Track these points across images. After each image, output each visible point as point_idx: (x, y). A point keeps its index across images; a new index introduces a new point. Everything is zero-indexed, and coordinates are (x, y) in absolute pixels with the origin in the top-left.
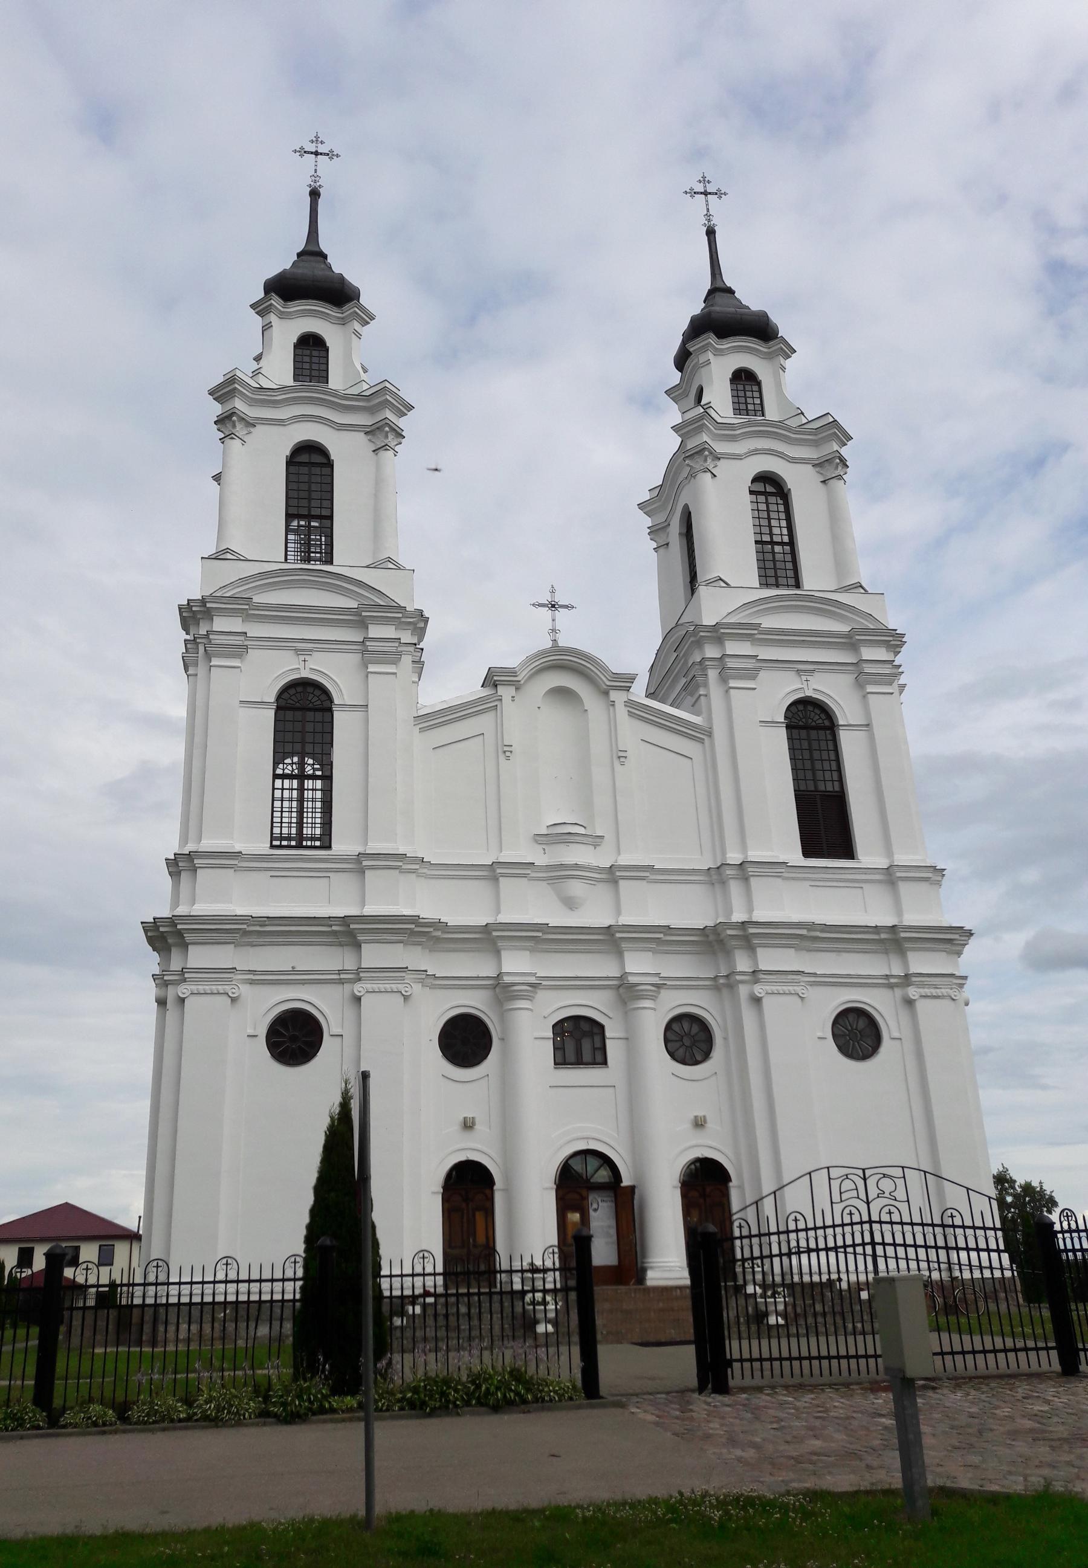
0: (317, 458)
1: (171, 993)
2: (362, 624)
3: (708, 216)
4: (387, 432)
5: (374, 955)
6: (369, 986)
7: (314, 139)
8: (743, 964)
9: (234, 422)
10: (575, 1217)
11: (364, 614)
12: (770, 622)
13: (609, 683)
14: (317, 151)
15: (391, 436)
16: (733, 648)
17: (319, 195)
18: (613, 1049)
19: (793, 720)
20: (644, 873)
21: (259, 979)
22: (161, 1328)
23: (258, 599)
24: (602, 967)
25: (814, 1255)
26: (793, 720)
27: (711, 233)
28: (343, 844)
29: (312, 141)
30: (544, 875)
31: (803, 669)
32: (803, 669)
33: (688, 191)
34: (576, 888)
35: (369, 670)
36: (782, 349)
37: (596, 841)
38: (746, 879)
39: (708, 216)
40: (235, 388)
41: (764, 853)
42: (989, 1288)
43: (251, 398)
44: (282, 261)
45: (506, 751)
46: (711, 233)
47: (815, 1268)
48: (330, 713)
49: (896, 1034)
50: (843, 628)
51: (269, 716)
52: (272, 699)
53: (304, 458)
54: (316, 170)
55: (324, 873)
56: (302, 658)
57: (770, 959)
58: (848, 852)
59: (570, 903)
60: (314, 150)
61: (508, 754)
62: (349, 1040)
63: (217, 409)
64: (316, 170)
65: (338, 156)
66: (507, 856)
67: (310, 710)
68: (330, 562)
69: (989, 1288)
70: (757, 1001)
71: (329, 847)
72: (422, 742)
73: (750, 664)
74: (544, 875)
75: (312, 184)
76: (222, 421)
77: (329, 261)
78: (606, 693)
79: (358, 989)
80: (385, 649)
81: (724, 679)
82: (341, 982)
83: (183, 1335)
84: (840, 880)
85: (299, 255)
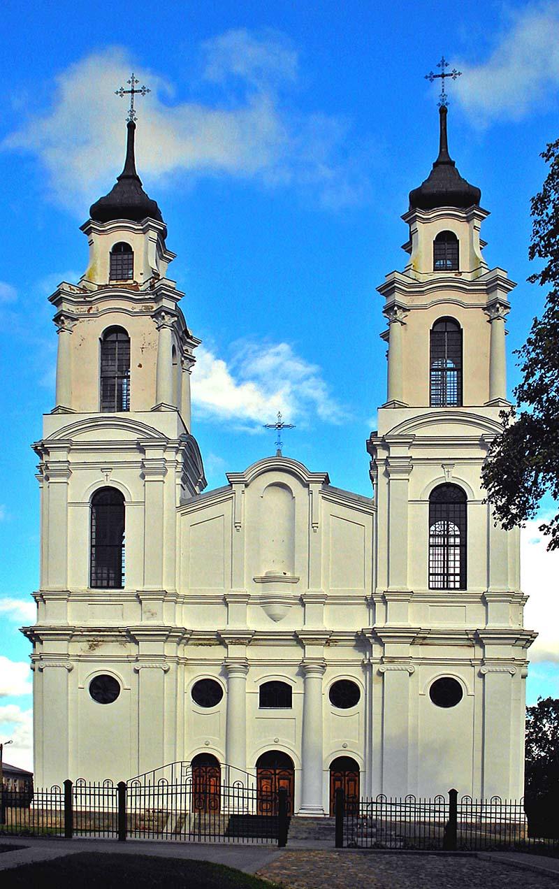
0: (451, 328)
1: (37, 664)
2: (142, 450)
3: (132, 112)
4: (396, 311)
5: (146, 648)
6: (141, 664)
7: (441, 63)
8: (377, 651)
9: (63, 321)
10: (338, 783)
11: (141, 444)
12: (420, 432)
13: (307, 479)
14: (443, 74)
15: (501, 309)
16: (396, 451)
17: (446, 111)
18: (296, 699)
19: (438, 498)
20: (322, 599)
21: (424, 661)
22: (41, 818)
23: (76, 438)
24: (295, 653)
25: (250, 800)
26: (438, 498)
27: (131, 127)
28: (476, 585)
29: (129, 82)
30: (259, 601)
31: (446, 463)
32: (106, 468)
33: (428, 75)
34: (277, 609)
35: (146, 479)
36: (149, 225)
37: (295, 581)
38: (385, 602)
39: (132, 112)
40: (61, 297)
41: (153, 587)
42: (389, 825)
43: (75, 302)
44: (419, 176)
45: (237, 526)
46: (131, 127)
47: (236, 805)
48: (464, 505)
49: (470, 693)
50: (134, 436)
51: (426, 507)
52: (87, 499)
53: (112, 337)
54: (443, 90)
55: (119, 601)
56: (105, 473)
57: (392, 649)
58: (119, 586)
59: (274, 618)
60: (440, 74)
61: (315, 528)
62: (134, 691)
63: (384, 301)
64: (443, 90)
65: (148, 91)
66: (235, 591)
67: (443, 503)
68: (460, 403)
69: (389, 825)
70: (381, 674)
71: (466, 589)
72: (183, 522)
73: (405, 463)
74: (259, 601)
75: (441, 102)
76: (57, 319)
77: (456, 167)
78: (308, 486)
79: (137, 665)
80: (62, 468)
81: (387, 474)
82: (129, 661)
83: (54, 822)
84: (452, 602)
85: (435, 165)
